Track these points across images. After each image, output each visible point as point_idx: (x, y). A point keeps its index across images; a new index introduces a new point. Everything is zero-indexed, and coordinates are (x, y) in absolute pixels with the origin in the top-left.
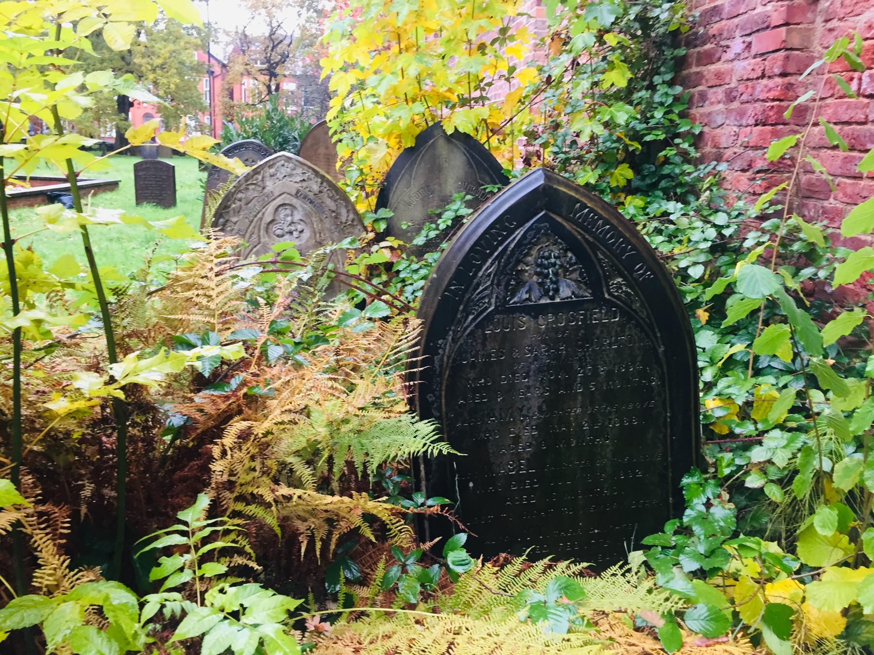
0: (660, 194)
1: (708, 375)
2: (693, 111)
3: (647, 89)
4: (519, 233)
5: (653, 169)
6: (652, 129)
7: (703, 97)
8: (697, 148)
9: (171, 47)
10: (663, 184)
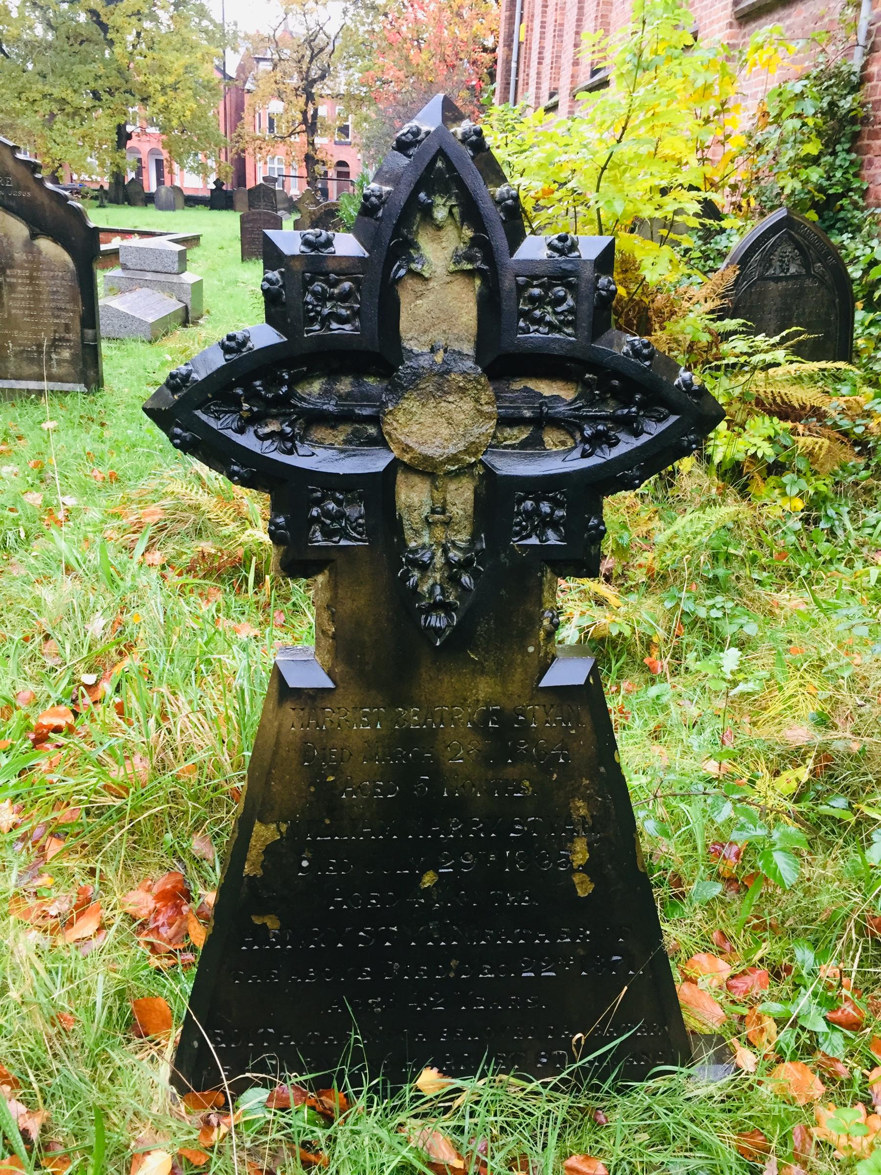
0: (836, 232)
1: (859, 331)
2: (863, 172)
3: (831, 154)
4: (773, 240)
5: (831, 214)
6: (833, 185)
7: (871, 163)
8: (864, 200)
9: (186, 59)
10: (838, 225)
